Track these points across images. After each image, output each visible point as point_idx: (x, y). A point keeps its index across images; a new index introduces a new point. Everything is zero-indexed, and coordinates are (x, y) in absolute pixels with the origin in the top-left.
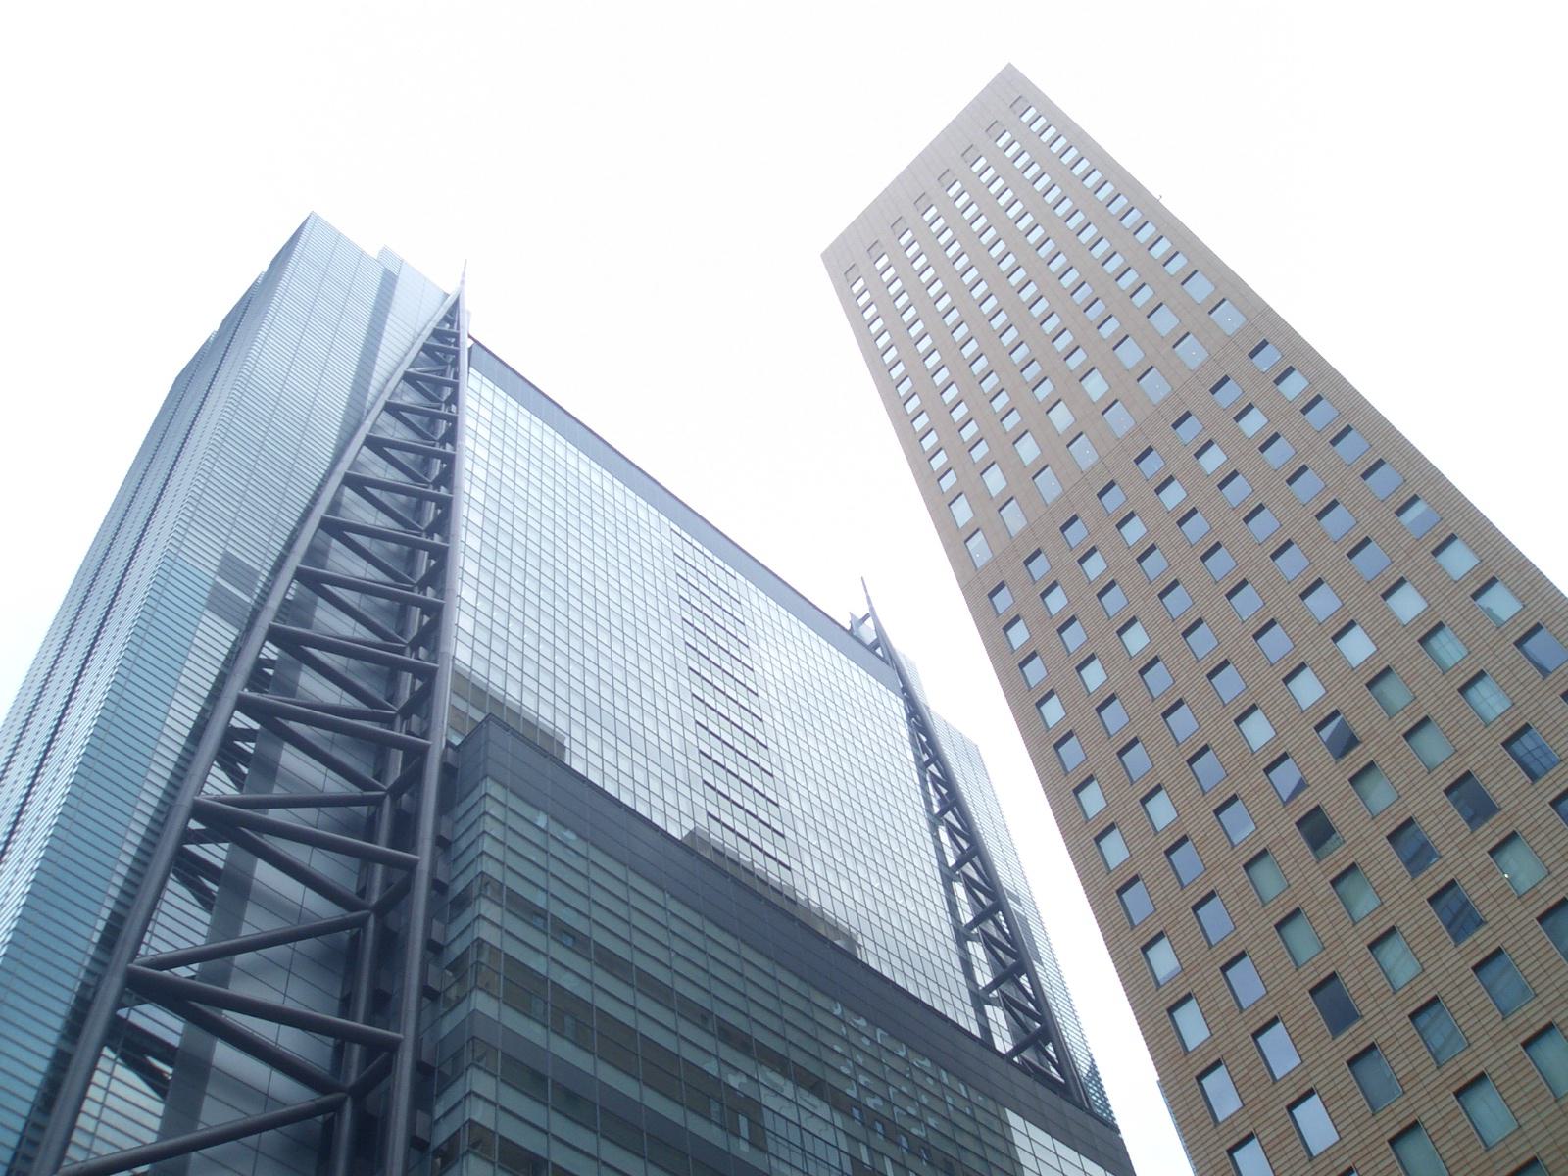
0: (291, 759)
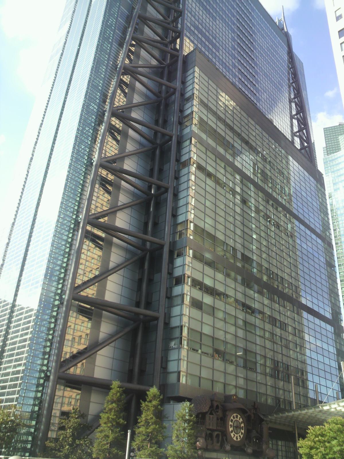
0: (147, 30)
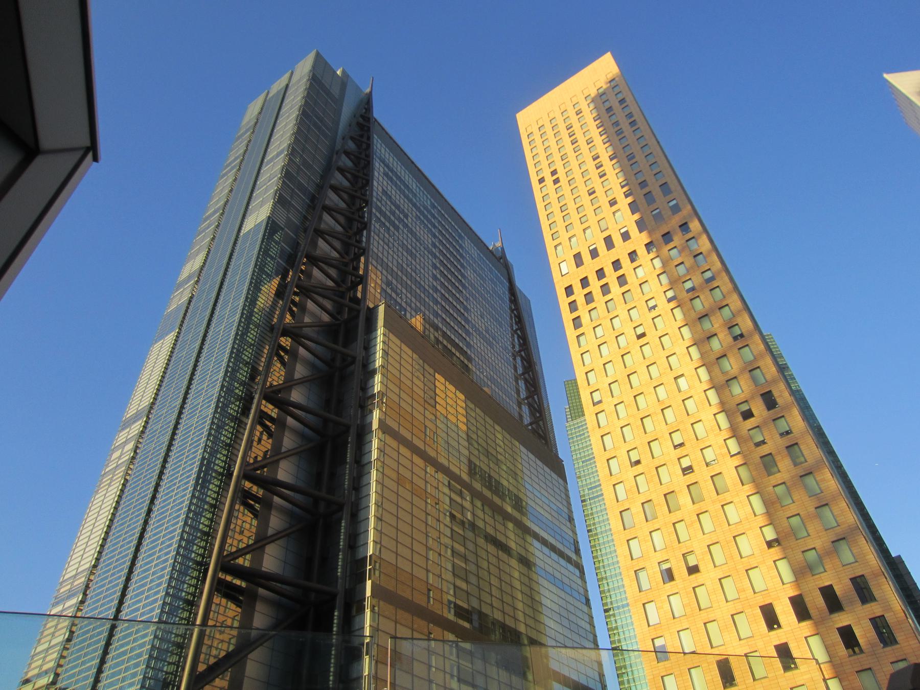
0: (316, 273)
